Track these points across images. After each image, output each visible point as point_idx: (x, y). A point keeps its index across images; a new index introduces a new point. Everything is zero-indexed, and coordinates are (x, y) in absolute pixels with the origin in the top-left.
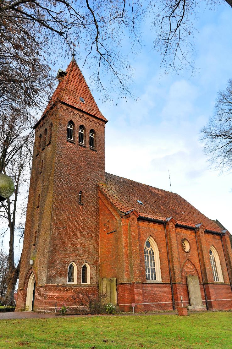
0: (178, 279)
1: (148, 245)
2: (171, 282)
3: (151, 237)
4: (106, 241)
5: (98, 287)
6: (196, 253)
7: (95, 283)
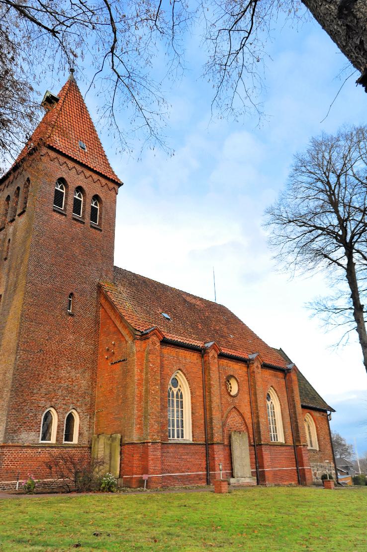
0: (217, 437)
1: (175, 383)
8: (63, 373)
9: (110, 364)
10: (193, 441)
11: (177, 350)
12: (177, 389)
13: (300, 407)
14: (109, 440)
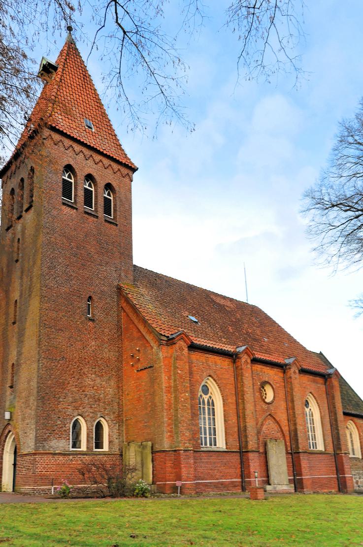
0: (252, 444)
1: (206, 390)
2: (240, 450)
3: (210, 378)
5: (121, 455)
6: (283, 405)
9: (136, 371)
11: (207, 355)
12: (208, 396)
13: (342, 414)
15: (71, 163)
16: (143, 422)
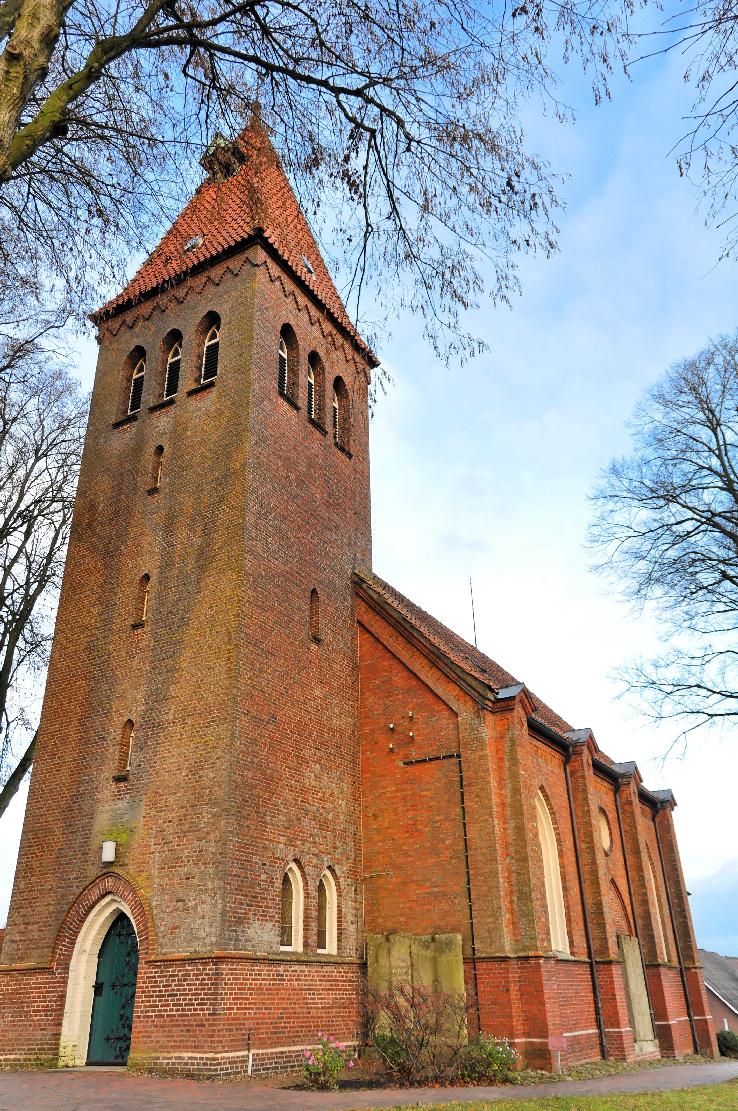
2: (590, 957)
4: (396, 791)
7: (351, 955)
8: (310, 780)
9: (401, 764)
10: (572, 953)
11: (539, 744)
14: (427, 948)
15: (292, 323)
16: (428, 884)
